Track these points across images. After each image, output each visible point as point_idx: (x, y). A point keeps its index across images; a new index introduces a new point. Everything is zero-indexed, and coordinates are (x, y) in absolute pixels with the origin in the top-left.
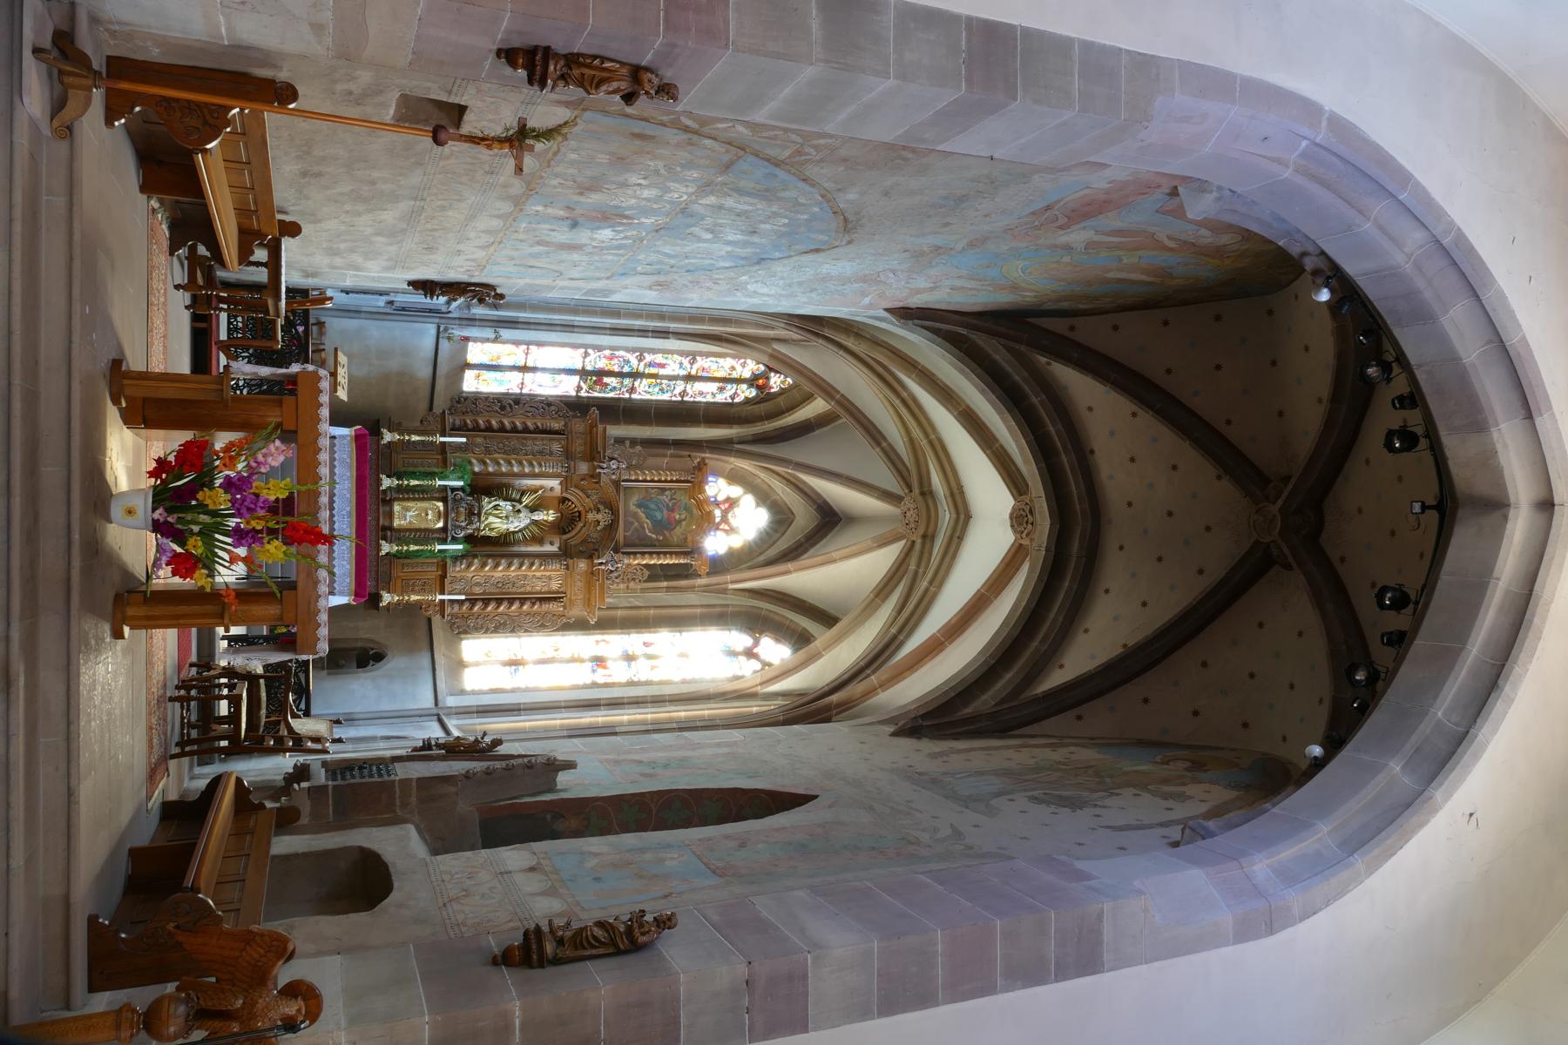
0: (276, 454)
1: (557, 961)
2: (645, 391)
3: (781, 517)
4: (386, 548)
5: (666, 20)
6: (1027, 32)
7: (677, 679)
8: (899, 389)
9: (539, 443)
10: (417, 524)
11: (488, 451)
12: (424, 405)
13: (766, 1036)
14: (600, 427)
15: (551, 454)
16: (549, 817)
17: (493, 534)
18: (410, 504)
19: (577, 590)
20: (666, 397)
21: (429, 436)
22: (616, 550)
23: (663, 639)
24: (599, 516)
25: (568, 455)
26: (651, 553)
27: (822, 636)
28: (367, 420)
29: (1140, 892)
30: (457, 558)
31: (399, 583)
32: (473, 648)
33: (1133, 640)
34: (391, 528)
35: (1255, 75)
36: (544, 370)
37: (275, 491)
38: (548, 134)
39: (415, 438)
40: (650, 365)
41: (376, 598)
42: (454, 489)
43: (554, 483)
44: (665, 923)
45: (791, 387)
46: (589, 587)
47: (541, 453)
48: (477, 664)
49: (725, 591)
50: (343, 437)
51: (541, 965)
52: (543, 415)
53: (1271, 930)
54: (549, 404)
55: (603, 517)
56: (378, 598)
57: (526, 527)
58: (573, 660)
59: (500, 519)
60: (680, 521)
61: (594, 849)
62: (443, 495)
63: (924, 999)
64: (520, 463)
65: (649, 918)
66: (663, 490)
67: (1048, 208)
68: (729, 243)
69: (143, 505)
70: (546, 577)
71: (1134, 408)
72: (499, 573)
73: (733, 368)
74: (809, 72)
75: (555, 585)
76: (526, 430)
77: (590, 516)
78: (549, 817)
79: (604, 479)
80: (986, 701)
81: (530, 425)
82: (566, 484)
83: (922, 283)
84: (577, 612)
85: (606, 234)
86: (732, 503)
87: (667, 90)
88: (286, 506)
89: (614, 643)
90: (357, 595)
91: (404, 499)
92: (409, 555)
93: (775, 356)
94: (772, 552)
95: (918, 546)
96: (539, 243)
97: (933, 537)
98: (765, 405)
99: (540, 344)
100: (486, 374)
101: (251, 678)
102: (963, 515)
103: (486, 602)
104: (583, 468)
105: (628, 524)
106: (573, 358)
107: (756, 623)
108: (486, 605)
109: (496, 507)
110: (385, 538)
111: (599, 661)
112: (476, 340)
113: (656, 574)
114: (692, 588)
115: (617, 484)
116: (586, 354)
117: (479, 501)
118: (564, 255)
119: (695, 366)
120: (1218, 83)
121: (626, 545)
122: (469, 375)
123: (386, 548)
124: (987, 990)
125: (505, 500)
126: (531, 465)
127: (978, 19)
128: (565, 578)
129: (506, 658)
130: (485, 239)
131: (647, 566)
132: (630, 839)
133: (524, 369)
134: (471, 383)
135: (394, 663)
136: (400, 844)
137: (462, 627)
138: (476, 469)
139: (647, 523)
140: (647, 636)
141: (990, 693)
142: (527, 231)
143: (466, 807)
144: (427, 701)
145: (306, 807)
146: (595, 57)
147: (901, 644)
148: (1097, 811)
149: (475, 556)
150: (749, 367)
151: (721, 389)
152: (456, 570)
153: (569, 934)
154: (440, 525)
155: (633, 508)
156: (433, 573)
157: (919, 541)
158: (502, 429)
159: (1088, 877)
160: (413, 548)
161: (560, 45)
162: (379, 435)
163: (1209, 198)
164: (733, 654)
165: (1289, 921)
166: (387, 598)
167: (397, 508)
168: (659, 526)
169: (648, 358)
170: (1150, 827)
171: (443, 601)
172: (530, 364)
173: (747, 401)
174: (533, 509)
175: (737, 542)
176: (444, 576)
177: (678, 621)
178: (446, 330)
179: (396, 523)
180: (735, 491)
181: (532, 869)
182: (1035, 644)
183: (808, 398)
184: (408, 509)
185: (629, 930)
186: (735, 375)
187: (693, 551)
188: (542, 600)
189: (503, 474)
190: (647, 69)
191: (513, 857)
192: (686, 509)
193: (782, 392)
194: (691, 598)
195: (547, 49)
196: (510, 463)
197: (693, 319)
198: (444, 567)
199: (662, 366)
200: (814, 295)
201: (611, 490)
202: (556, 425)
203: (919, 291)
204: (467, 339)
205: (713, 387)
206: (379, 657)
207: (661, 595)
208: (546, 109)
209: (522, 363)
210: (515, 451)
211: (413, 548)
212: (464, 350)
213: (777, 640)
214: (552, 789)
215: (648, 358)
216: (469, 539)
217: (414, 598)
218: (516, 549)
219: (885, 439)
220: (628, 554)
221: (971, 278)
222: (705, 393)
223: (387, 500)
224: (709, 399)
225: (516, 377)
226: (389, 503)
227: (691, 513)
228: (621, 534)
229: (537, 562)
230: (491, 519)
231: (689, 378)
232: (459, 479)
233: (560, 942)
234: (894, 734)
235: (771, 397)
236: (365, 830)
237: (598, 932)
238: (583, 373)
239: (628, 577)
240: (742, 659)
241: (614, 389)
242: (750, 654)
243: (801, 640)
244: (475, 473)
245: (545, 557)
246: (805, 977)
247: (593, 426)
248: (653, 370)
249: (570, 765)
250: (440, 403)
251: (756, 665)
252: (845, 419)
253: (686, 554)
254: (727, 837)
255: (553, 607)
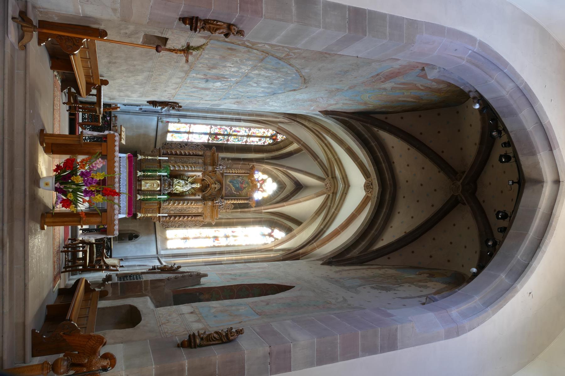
0: (99, 163)
1: (201, 346)
2: (232, 141)
3: (282, 186)
4: (139, 197)
5: (240, 7)
6: (370, 12)
7: (244, 244)
8: (324, 140)
9: (194, 159)
10: (150, 189)
11: (176, 162)
12: (153, 146)
13: (276, 373)
14: (216, 154)
15: (199, 163)
16: (198, 294)
17: (178, 192)
18: (148, 181)
19: (208, 212)
20: (240, 143)
21: (155, 157)
22: (222, 198)
23: (239, 230)
24: (216, 186)
25: (205, 164)
26: (234, 199)
27: (296, 229)
28: (132, 151)
29: (411, 321)
30: (165, 201)
31: (144, 210)
32: (170, 233)
33: (408, 230)
34: (141, 190)
35: (452, 27)
36: (196, 133)
37: (99, 177)
38: (197, 48)
39: (150, 158)
40: (234, 131)
41: (135, 215)
42: (163, 176)
43: (200, 174)
44: (240, 332)
45: (285, 139)
46: (212, 211)
47: (195, 163)
48: (172, 239)
49: (261, 213)
50: (124, 157)
51: (195, 347)
52: (195, 149)
53: (458, 335)
54: (198, 146)
55: (217, 186)
56: (136, 215)
57: (190, 190)
58: (206, 237)
59: (180, 187)
60: (245, 188)
61: (214, 306)
62: (160, 178)
63: (333, 360)
64: (187, 167)
65: (234, 330)
66: (239, 176)
67: (378, 75)
68: (263, 87)
69: (52, 182)
70: (197, 208)
71: (409, 147)
72: (180, 206)
73: (264, 133)
74: (292, 26)
75: (200, 211)
76: (190, 155)
77: (213, 186)
78: (198, 294)
79: (218, 172)
80: (355, 252)
81: (191, 153)
82: (204, 174)
83: (332, 102)
84: (208, 220)
85: (218, 84)
86: (264, 181)
87: (240, 33)
88: (103, 182)
89: (221, 232)
90: (129, 214)
91: (145, 180)
92: (147, 200)
93: (279, 128)
94: (278, 199)
95: (331, 197)
96: (194, 87)
97: (336, 193)
98: (276, 146)
99: (194, 124)
100: (175, 135)
101: (91, 244)
102: (347, 185)
103: (175, 217)
104: (210, 168)
105: (226, 189)
106: (206, 129)
107: (272, 224)
108: (175, 218)
109: (179, 183)
110: (139, 194)
111: (216, 238)
112: (171, 122)
113: (236, 206)
114: (249, 212)
115: (222, 174)
116: (211, 128)
117: (173, 180)
118: (203, 92)
119: (251, 132)
120: (439, 30)
121: (226, 196)
122: (169, 135)
123: (139, 197)
124: (356, 356)
125: (182, 180)
126: (191, 167)
127: (352, 7)
128: (204, 208)
129: (182, 237)
130: (175, 86)
131: (233, 204)
132: (227, 302)
133: (189, 133)
134: (170, 138)
135: (142, 239)
136: (144, 304)
137: (167, 225)
138: (172, 169)
139: (233, 188)
140: (233, 229)
141: (357, 249)
142: (190, 83)
143: (168, 290)
144: (154, 252)
145: (110, 290)
146: (214, 21)
147: (325, 232)
148: (395, 292)
149: (171, 200)
150: (270, 132)
151: (260, 140)
152: (164, 205)
153: (205, 336)
154: (159, 189)
155: (228, 183)
156: (156, 206)
157: (331, 195)
158: (181, 154)
159: (392, 316)
160: (149, 197)
161: (202, 16)
162: (137, 156)
163: (436, 71)
164: (264, 235)
165: (464, 331)
166: (139, 215)
167: (143, 183)
168: (237, 189)
169: (234, 129)
170: (414, 297)
171: (159, 216)
172: (191, 131)
173: (269, 144)
174: (192, 183)
175: (265, 195)
176: (160, 207)
177: (244, 223)
178: (161, 119)
179: (143, 188)
180: (265, 177)
181: (192, 313)
182: (373, 232)
183: (291, 143)
184: (147, 183)
185: (227, 335)
186: (265, 135)
187: (250, 198)
188: (195, 216)
189: (181, 171)
190: (233, 25)
191: (185, 308)
192: (247, 183)
193: (282, 141)
194: (249, 215)
195: (197, 18)
196: (184, 167)
197: (250, 115)
198: (160, 204)
199: (239, 132)
200: (293, 106)
201: (220, 176)
202: (200, 153)
203: (331, 105)
204: (168, 122)
205: (257, 139)
206: (137, 237)
207: (238, 214)
208: (197, 39)
209: (188, 131)
210: (185, 162)
211: (149, 197)
212: (167, 126)
213: (280, 230)
214: (199, 284)
215: (234, 129)
216: (169, 194)
217: (149, 215)
218: (186, 197)
219: (319, 158)
220: (226, 199)
221: (350, 100)
222: (254, 141)
223: (139, 180)
224: (256, 143)
225: (186, 136)
226: (140, 181)
227: (249, 185)
228: (224, 192)
229: (193, 202)
230: (177, 187)
231: (248, 136)
232: (166, 172)
233: (202, 339)
234: (322, 264)
235: (278, 143)
236: (132, 299)
237: (216, 335)
238: (210, 134)
239: (226, 207)
240: (268, 237)
241: (221, 140)
242: (270, 235)
243: (289, 230)
244: (171, 170)
245: (196, 201)
246: (290, 351)
247: (214, 153)
248: (235, 133)
249: (205, 275)
250: (159, 145)
251: (272, 239)
252: (304, 151)
253: (247, 199)
254: (262, 301)
255: (199, 218)
